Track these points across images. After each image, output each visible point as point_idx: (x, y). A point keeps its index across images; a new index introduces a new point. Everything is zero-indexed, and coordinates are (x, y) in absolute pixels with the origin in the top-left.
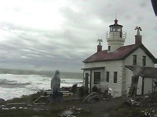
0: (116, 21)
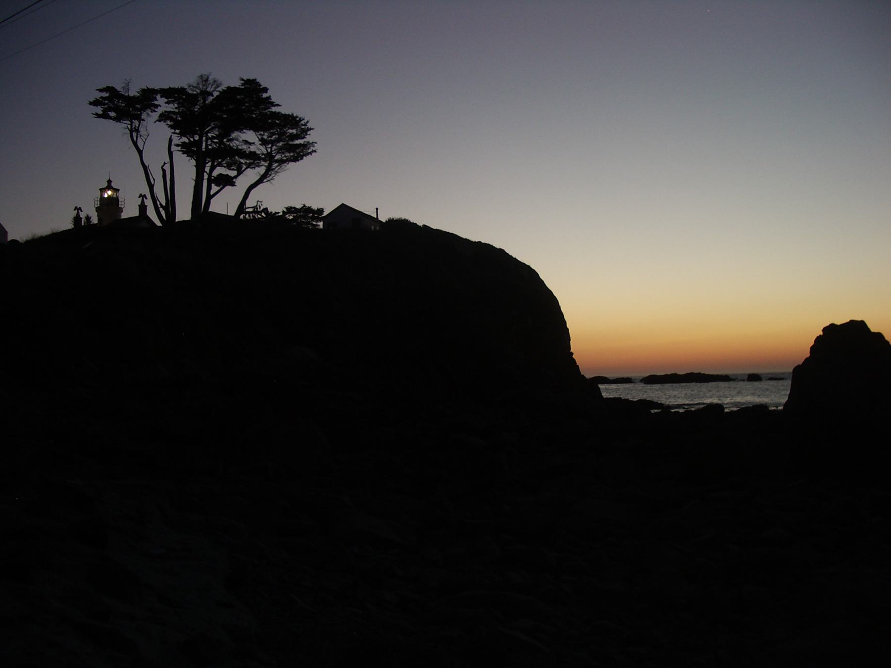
0: (109, 182)
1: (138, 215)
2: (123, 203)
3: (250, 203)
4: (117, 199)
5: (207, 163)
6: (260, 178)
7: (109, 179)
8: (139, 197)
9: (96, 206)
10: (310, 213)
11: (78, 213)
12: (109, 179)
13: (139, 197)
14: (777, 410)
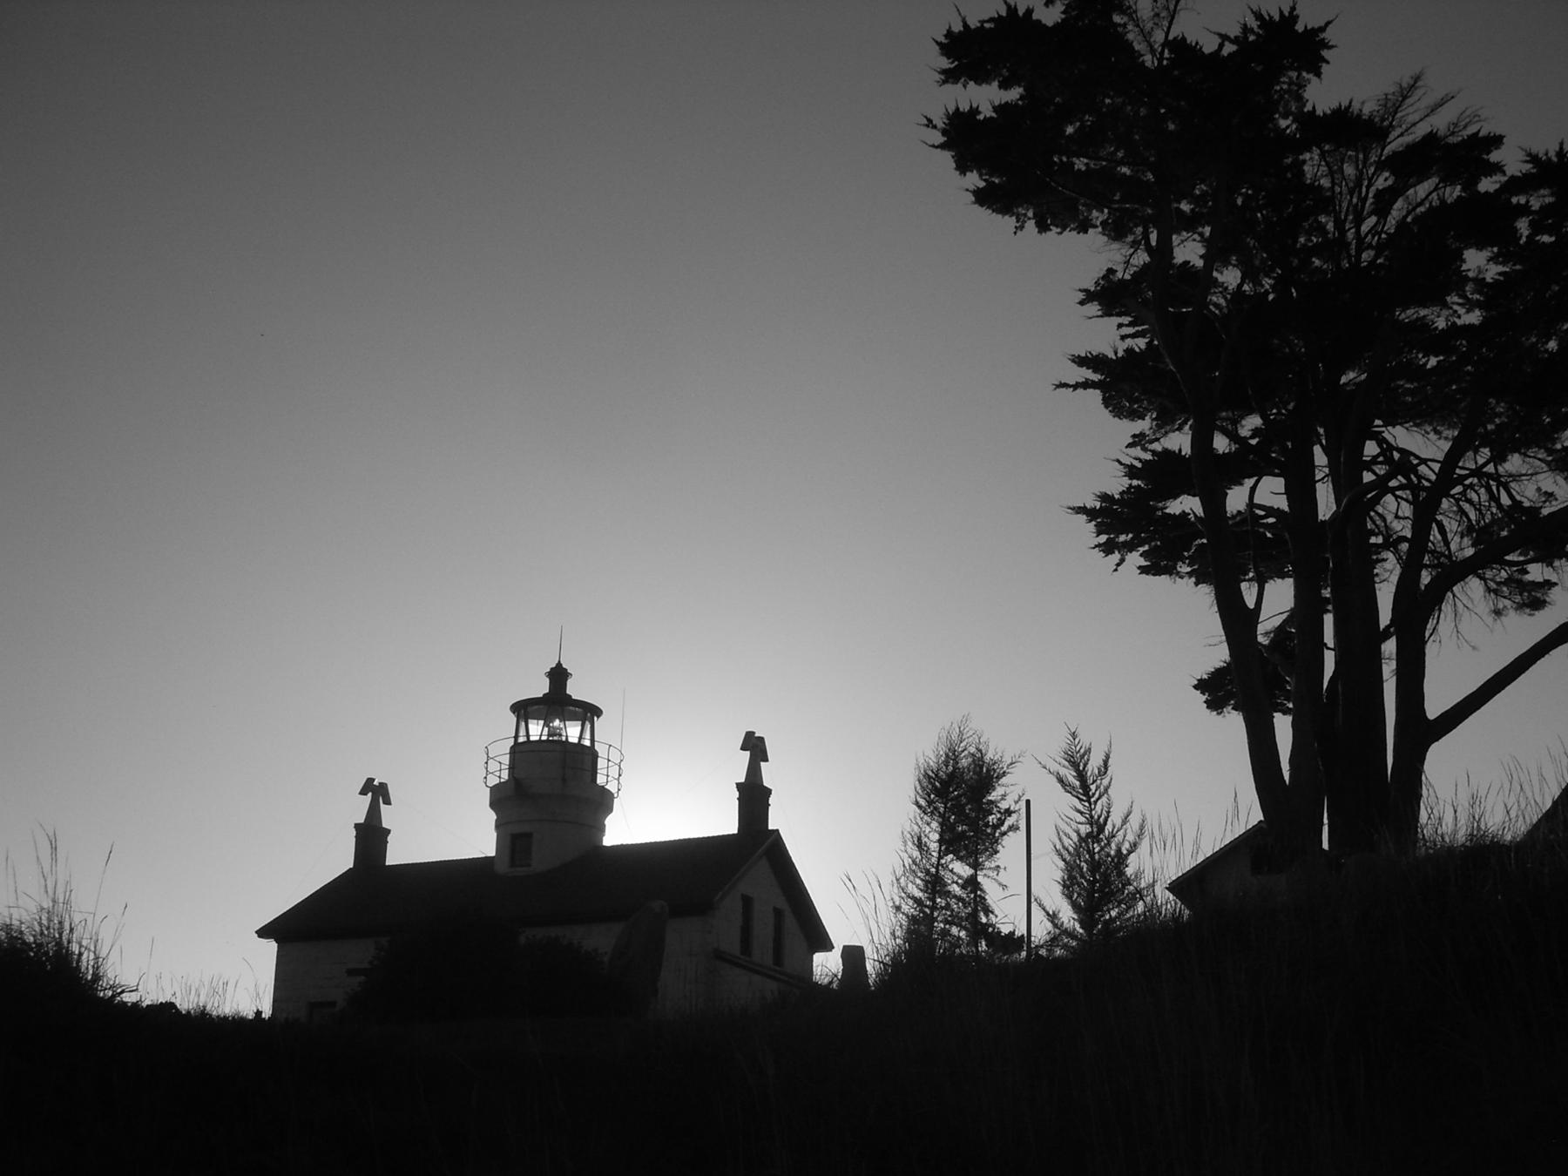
0: (558, 676)
1: (736, 832)
2: (614, 772)
3: (1100, 313)
4: (584, 758)
5: (1270, 278)
6: (1397, 679)
7: (559, 664)
8: (363, 792)
9: (493, 781)
10: (1479, 443)
11: (374, 812)
12: (559, 664)
13: (363, 792)
14: (1326, 436)
